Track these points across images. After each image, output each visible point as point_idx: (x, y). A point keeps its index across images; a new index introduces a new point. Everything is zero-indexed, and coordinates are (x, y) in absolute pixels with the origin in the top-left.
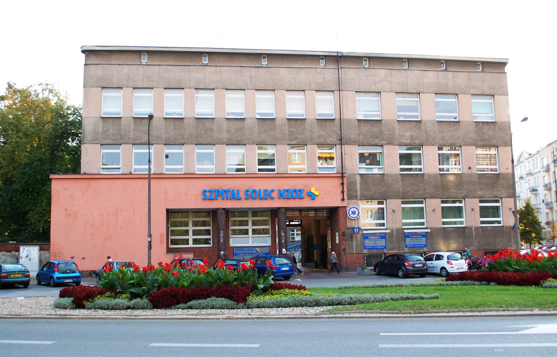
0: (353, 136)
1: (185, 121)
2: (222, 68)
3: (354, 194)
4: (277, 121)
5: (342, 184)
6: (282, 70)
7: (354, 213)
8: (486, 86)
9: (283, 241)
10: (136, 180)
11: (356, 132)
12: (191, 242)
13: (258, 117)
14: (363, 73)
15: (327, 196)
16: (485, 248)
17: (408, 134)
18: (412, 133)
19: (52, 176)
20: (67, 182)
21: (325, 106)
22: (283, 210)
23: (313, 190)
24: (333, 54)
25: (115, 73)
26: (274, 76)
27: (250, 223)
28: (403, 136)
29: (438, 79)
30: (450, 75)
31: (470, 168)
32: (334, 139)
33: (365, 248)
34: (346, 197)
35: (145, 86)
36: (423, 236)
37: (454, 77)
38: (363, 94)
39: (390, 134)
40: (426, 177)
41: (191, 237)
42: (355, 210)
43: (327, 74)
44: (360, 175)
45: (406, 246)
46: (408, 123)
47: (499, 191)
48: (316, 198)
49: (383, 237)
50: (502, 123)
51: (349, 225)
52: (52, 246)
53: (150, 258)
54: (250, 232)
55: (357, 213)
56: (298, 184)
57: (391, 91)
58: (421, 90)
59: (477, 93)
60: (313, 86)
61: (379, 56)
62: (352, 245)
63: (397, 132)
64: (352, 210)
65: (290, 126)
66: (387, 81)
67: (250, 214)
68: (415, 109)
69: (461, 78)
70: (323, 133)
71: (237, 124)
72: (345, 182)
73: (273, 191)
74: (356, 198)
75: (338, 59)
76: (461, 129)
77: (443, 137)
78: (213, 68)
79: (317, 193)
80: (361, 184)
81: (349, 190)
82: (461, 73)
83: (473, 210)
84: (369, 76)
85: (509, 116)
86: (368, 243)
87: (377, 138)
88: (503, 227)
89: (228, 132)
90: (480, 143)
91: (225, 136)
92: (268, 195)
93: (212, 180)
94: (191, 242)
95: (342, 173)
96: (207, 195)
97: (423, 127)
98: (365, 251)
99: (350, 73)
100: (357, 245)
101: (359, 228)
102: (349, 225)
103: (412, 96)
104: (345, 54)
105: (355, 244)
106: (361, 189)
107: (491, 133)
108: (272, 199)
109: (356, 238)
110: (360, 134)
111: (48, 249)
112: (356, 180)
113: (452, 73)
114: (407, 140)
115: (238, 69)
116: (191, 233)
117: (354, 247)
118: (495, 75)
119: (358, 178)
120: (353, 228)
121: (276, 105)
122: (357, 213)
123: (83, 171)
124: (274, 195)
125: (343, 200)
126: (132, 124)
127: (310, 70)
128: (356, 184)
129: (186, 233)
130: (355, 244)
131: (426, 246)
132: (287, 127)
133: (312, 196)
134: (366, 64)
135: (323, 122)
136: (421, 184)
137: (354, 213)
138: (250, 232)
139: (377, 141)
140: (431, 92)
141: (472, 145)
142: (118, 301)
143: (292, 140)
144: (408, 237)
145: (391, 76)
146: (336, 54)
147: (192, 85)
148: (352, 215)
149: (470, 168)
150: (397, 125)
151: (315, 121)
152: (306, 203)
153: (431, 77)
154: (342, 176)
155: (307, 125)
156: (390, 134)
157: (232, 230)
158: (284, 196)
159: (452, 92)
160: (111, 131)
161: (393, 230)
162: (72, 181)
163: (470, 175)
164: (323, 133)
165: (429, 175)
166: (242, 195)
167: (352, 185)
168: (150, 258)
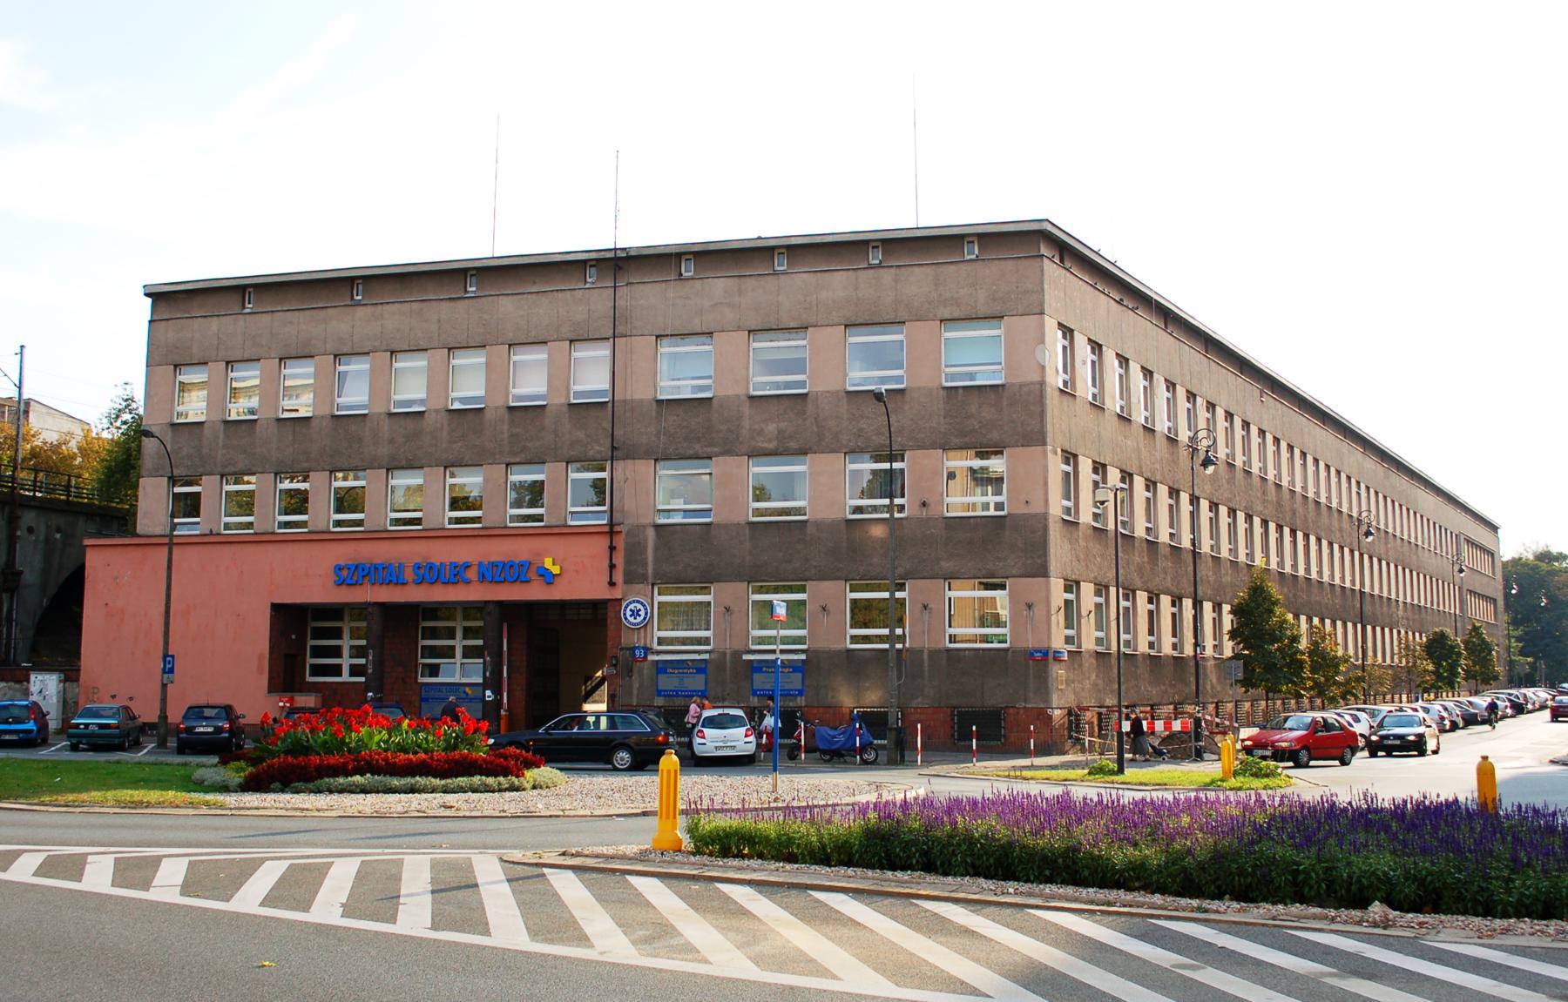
0: (644, 440)
1: (314, 423)
2: (386, 307)
3: (640, 571)
4: (488, 414)
5: (612, 548)
6: (504, 301)
7: (635, 613)
8: (981, 296)
9: (599, 674)
10: (449, 541)
11: (652, 429)
12: (346, 670)
13: (457, 406)
14: (674, 292)
15: (575, 575)
16: (954, 702)
17: (772, 428)
18: (783, 425)
19: (87, 542)
20: (108, 553)
21: (591, 374)
22: (491, 606)
23: (548, 563)
24: (609, 255)
25: (197, 335)
26: (486, 317)
27: (459, 634)
28: (761, 433)
29: (856, 289)
30: (887, 276)
31: (924, 504)
32: (603, 447)
33: (659, 693)
34: (619, 577)
35: (246, 356)
36: (796, 670)
37: (896, 281)
38: (678, 340)
39: (729, 430)
40: (810, 529)
41: (346, 662)
42: (639, 606)
43: (593, 299)
44: (658, 527)
45: (754, 694)
46: (775, 401)
47: (999, 559)
48: (557, 580)
49: (700, 671)
50: (1021, 385)
51: (624, 641)
52: (82, 673)
53: (164, 700)
54: (459, 652)
55: (642, 613)
56: (519, 550)
57: (739, 329)
58: (813, 320)
59: (956, 315)
60: (566, 331)
61: (712, 247)
62: (631, 687)
63: (746, 423)
64: (632, 607)
65: (512, 422)
66: (729, 305)
67: (459, 615)
68: (796, 366)
69: (917, 280)
70: (581, 435)
71: (410, 424)
72: (620, 542)
73: (467, 566)
74: (642, 578)
75: (618, 265)
76: (907, 407)
77: (861, 430)
78: (369, 309)
79: (556, 570)
80: (656, 549)
81: (628, 562)
82: (917, 270)
83: (925, 607)
84: (688, 298)
85: (1043, 367)
86: (666, 683)
87: (699, 440)
88: (1006, 650)
89: (391, 441)
90: (957, 441)
91: (384, 451)
92: (457, 574)
93: (353, 545)
94: (346, 670)
95: (611, 524)
96: (350, 575)
97: (810, 408)
98: (659, 701)
99: (649, 298)
100: (641, 686)
101: (648, 650)
102: (624, 641)
103: (793, 336)
104: (632, 253)
105: (636, 685)
106: (656, 559)
107: (987, 414)
108: (469, 582)
109: (640, 671)
110: (659, 432)
111: (77, 680)
112: (646, 540)
113: (892, 270)
114: (770, 441)
115: (416, 306)
116: (346, 652)
117: (635, 692)
118: (1010, 265)
119: (651, 533)
120: (633, 649)
121: (488, 380)
122: (642, 613)
123: (139, 530)
124: (472, 574)
125: (612, 584)
126: (222, 436)
127: (560, 295)
128: (645, 548)
129: (336, 652)
130: (636, 685)
131: (801, 693)
132: (506, 427)
133: (548, 578)
134: (781, 265)
135: (581, 410)
136: (799, 547)
137: (635, 613)
138: (459, 652)
139: (698, 448)
140: (836, 321)
141: (933, 446)
142: (1138, 796)
143: (515, 454)
144: (759, 670)
145: (740, 292)
146: (611, 255)
147: (330, 347)
148: (631, 619)
149: (924, 504)
150: (746, 409)
151: (565, 409)
152: (535, 592)
153: (838, 284)
154: (611, 531)
155: (548, 421)
156: (729, 430)
157: (313, 647)
158: (489, 576)
159: (891, 317)
160: (185, 451)
161: (724, 654)
162: (119, 550)
163: (926, 522)
164: (581, 435)
165: (818, 525)
166: (409, 575)
167: (635, 551)
168: (164, 700)
